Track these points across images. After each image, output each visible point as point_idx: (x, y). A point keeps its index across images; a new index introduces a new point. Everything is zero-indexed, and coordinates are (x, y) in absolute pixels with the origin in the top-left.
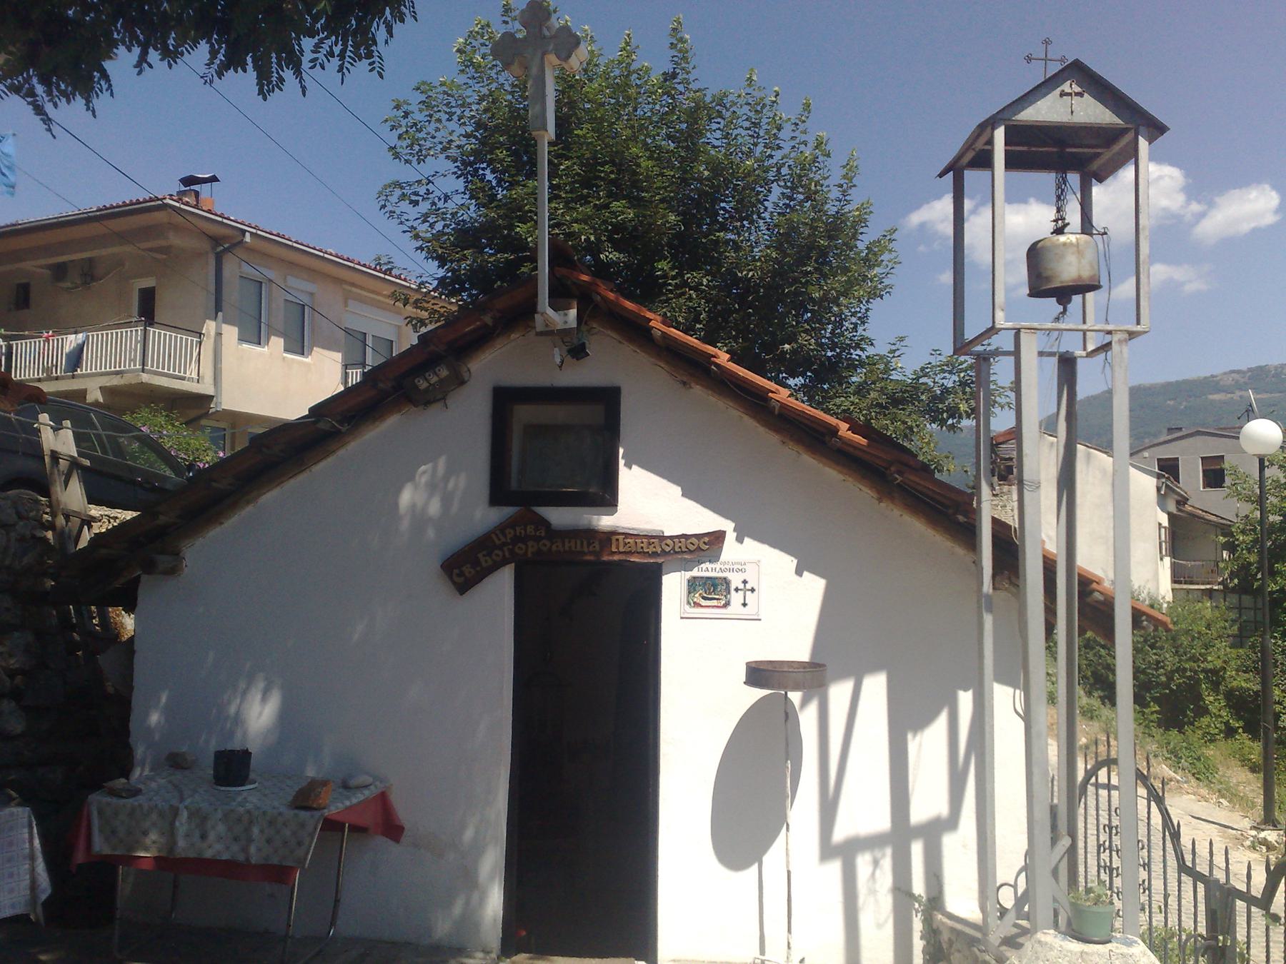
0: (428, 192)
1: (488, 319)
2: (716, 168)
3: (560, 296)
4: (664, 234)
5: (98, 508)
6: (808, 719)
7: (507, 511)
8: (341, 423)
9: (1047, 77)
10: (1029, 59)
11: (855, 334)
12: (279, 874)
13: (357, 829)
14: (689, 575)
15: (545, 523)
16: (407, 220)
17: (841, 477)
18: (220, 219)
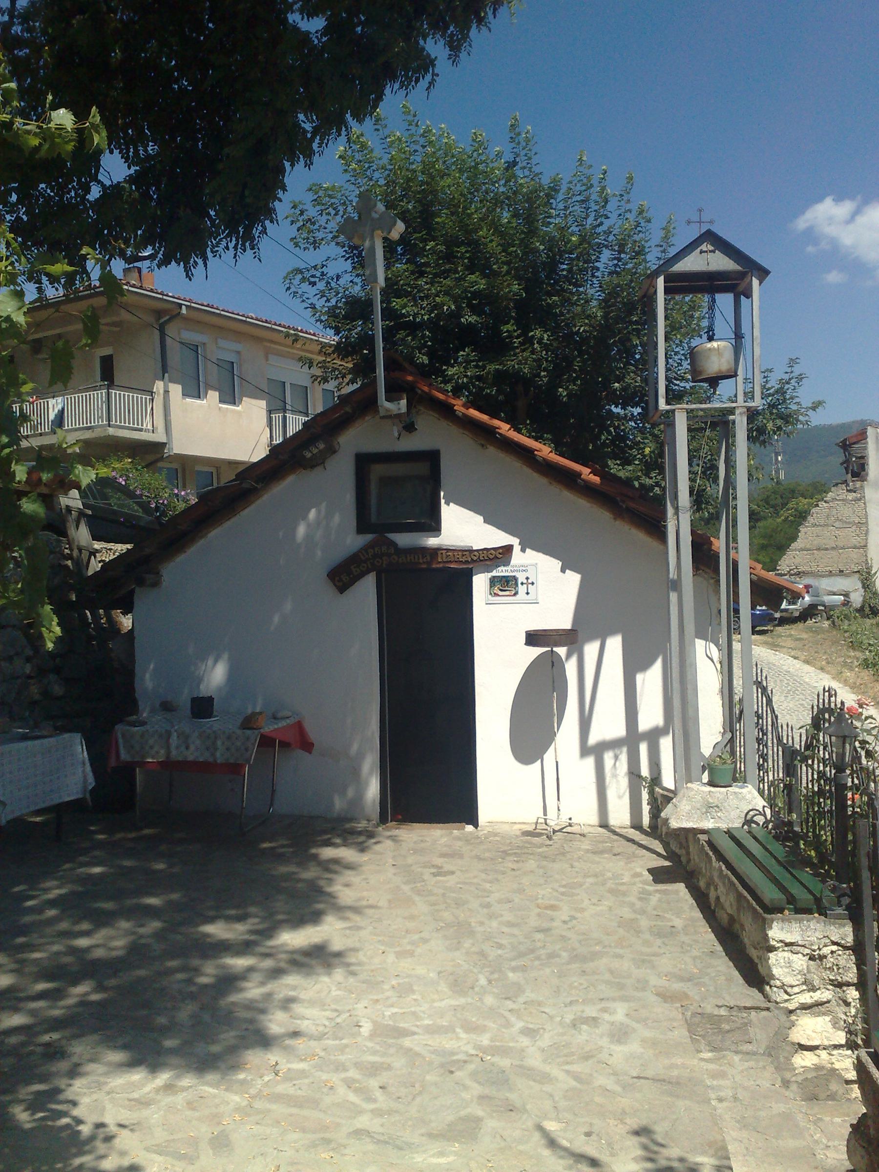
0: (323, 274)
1: (348, 409)
2: (551, 244)
3: (393, 391)
4: (511, 299)
5: (99, 543)
6: (571, 668)
7: (369, 537)
8: (257, 482)
9: (702, 232)
10: (689, 222)
11: (680, 368)
12: (235, 769)
13: (285, 745)
14: (490, 575)
15: (393, 544)
16: (308, 299)
17: (588, 505)
18: (160, 296)
